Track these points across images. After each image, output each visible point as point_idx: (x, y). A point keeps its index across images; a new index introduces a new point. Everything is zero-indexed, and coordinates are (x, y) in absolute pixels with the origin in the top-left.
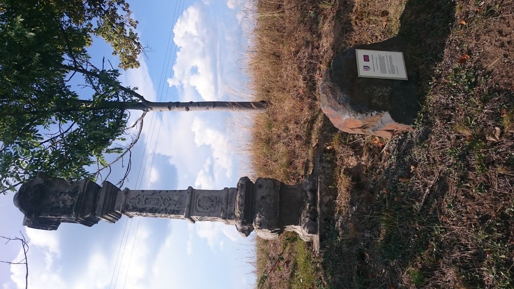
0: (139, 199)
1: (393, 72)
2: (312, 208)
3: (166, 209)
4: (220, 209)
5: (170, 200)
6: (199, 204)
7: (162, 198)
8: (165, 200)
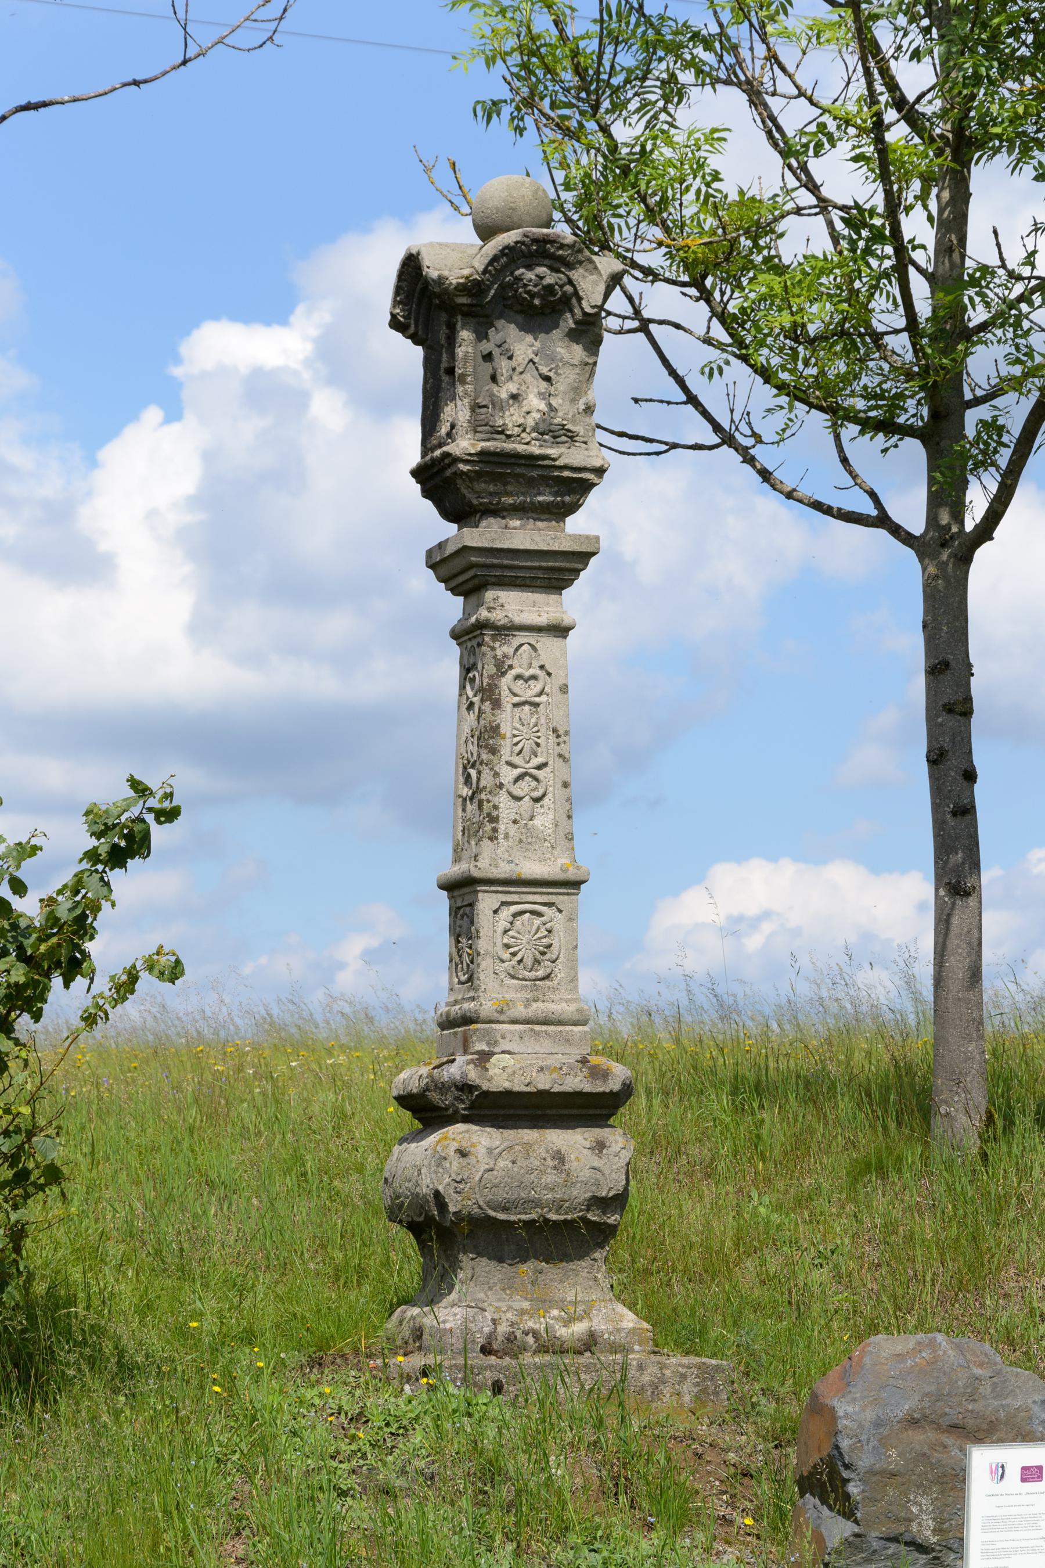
0: (534, 677)
1: (987, 1555)
2: (530, 1340)
3: (501, 786)
4: (508, 997)
5: (537, 800)
6: (522, 913)
7: (539, 767)
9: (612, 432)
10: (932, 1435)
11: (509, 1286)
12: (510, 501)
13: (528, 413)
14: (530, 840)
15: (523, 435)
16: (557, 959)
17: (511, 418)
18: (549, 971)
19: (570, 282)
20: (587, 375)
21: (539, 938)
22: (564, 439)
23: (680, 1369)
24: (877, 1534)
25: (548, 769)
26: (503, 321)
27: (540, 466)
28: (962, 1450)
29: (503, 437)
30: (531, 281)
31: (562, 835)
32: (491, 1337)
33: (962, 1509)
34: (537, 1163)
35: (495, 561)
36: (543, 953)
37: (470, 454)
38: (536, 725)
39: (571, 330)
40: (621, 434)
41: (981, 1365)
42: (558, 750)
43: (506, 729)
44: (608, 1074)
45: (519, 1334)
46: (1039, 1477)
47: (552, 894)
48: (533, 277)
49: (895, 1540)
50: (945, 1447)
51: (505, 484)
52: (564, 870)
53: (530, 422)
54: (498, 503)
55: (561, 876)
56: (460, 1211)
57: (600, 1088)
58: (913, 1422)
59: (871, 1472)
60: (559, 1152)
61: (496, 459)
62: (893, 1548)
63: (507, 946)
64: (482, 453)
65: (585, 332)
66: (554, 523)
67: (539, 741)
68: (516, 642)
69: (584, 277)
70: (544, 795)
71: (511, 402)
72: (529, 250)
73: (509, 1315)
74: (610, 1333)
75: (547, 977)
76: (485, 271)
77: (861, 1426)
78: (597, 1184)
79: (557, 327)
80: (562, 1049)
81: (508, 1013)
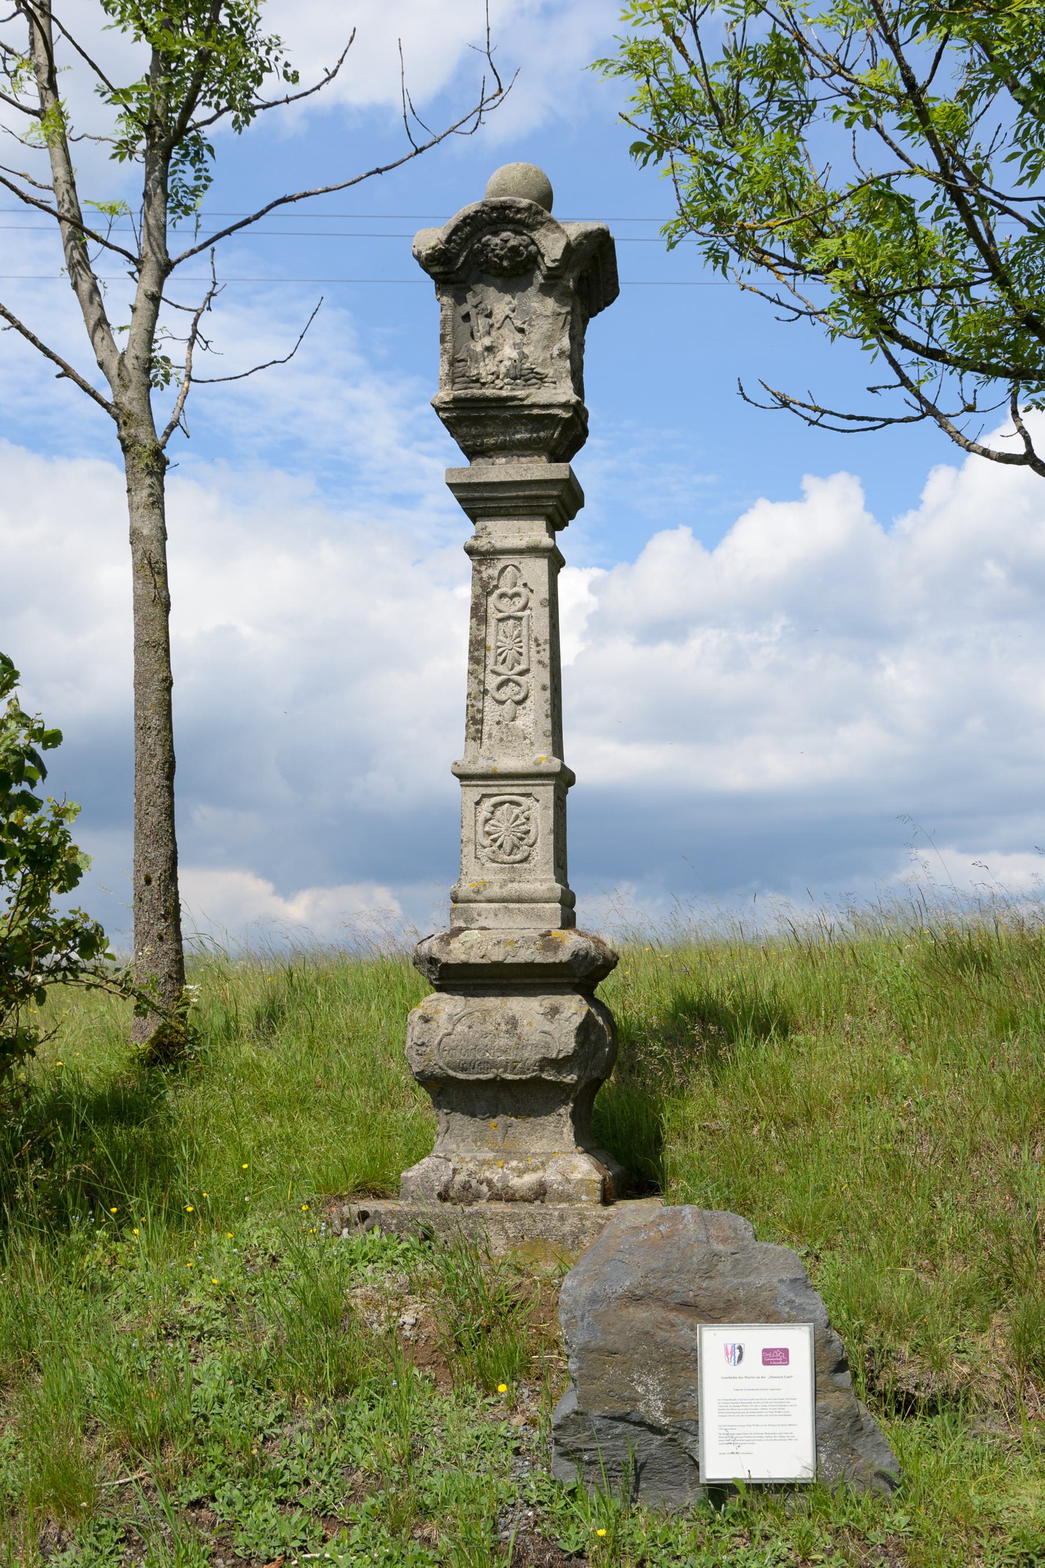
0: (517, 595)
2: (484, 1188)
4: (487, 878)
5: (519, 703)
6: (502, 803)
7: (521, 674)
8: (518, 684)
9: (843, 417)
10: (658, 1313)
11: (480, 1139)
12: (492, 441)
13: (501, 362)
14: (510, 738)
15: (497, 382)
16: (534, 843)
17: (485, 369)
18: (526, 854)
19: (533, 242)
20: (561, 324)
21: (518, 826)
22: (534, 381)
23: (600, 1221)
24: (599, 1413)
25: (530, 675)
26: (481, 285)
27: (509, 406)
28: (693, 1329)
29: (478, 385)
30: (497, 245)
31: (540, 732)
32: (447, 1188)
33: (695, 1390)
34: (492, 1028)
35: (476, 495)
36: (522, 839)
37: (445, 403)
38: (519, 636)
39: (542, 285)
40: (851, 417)
41: (724, 1240)
42: (538, 657)
43: (491, 642)
44: (559, 947)
45: (474, 1183)
46: (784, 1360)
47: (528, 785)
48: (499, 242)
49: (622, 1419)
50: (673, 1326)
51: (485, 427)
52: (536, 764)
53: (503, 370)
54: (482, 444)
55: (534, 769)
56: (423, 1071)
57: (551, 959)
58: (635, 1299)
59: (586, 1350)
60: (514, 1018)
61: (469, 405)
62: (620, 1428)
63: (489, 834)
64: (456, 400)
65: (554, 286)
66: (536, 457)
67: (520, 650)
68: (500, 565)
69: (546, 236)
70: (526, 698)
71: (486, 354)
72: (491, 218)
73: (471, 1166)
74: (560, 1183)
75: (525, 860)
76: (449, 240)
77: (576, 1302)
78: (547, 1046)
79: (531, 284)
80: (534, 925)
81: (484, 893)
